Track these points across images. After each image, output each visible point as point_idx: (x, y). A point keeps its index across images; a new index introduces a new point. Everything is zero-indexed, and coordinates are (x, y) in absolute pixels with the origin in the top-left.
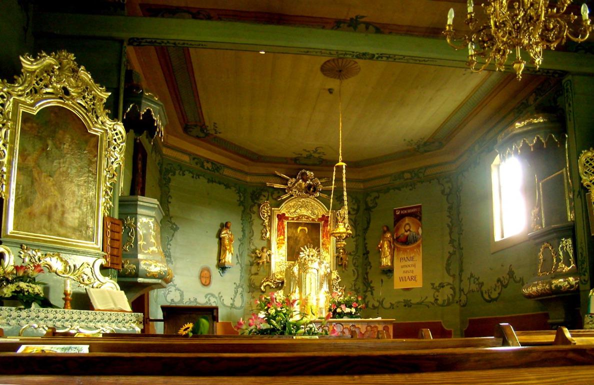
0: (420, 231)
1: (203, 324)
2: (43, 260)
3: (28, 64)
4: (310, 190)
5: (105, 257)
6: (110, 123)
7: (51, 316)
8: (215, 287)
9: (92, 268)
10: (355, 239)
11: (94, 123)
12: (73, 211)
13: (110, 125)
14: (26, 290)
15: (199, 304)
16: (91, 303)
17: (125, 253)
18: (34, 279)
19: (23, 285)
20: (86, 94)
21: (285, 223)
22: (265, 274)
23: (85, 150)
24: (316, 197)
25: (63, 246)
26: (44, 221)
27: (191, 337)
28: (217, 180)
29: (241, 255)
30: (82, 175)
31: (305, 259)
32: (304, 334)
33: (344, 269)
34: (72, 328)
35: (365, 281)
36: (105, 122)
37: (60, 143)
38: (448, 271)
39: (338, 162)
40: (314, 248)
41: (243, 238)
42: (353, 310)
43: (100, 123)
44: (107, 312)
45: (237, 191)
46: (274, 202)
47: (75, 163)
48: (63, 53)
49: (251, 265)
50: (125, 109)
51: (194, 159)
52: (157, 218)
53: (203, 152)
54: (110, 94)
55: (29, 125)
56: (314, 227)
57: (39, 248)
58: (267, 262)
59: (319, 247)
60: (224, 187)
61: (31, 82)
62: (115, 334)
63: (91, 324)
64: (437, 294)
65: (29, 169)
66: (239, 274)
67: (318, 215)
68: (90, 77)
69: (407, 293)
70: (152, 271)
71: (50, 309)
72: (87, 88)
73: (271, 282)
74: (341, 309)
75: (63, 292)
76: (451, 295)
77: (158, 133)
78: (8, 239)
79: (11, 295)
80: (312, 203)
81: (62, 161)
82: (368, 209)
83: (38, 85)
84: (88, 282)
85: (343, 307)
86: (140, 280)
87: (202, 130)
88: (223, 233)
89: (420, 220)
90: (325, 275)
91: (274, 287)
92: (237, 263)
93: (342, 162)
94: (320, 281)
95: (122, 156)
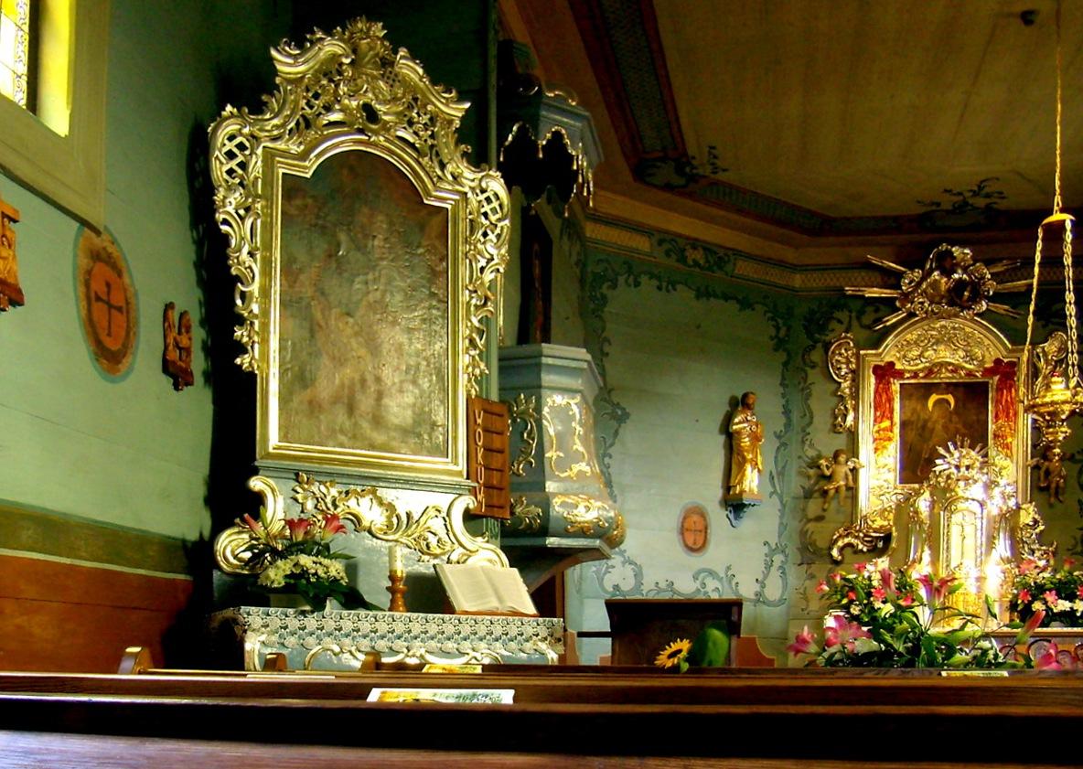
1: (715, 644)
2: (341, 505)
3: (287, 64)
4: (960, 297)
5: (473, 492)
6: (472, 176)
7: (365, 627)
8: (716, 555)
9: (447, 519)
11: (435, 179)
12: (401, 391)
13: (473, 180)
14: (313, 571)
15: (679, 594)
16: (448, 598)
17: (515, 479)
18: (327, 547)
19: (305, 560)
20: (414, 114)
21: (896, 386)
22: (841, 518)
23: (418, 247)
24: (978, 315)
25: (382, 472)
26: (341, 417)
27: (686, 673)
29: (781, 474)
30: (416, 305)
31: (949, 477)
32: (966, 665)
33: (1052, 500)
34: (410, 654)
36: (461, 175)
37: (366, 236)
39: (1050, 213)
40: (972, 447)
41: (786, 433)
43: (450, 178)
44: (483, 617)
45: (769, 315)
46: (864, 334)
47: (398, 278)
48: (360, 25)
49: (806, 497)
50: (502, 138)
51: (660, 242)
52: (586, 393)
53: (680, 224)
54: (467, 105)
55: (298, 202)
56: (972, 393)
57: (333, 477)
58: (849, 488)
59: (985, 445)
60: (738, 306)
61: (296, 102)
62: (504, 665)
63: (450, 645)
65: (304, 303)
66: (777, 521)
67: (982, 362)
68: (421, 71)
70: (579, 519)
71: (362, 612)
72: (415, 99)
73: (857, 537)
74: (1046, 603)
75: (388, 574)
77: (581, 188)
78: (269, 463)
79: (283, 584)
80: (968, 329)
81: (370, 277)
83: (311, 107)
84: (438, 551)
85: (1050, 597)
86: (552, 541)
87: (680, 170)
88: (736, 420)
91: (865, 549)
92: (771, 494)
93: (1062, 211)
95: (503, 251)
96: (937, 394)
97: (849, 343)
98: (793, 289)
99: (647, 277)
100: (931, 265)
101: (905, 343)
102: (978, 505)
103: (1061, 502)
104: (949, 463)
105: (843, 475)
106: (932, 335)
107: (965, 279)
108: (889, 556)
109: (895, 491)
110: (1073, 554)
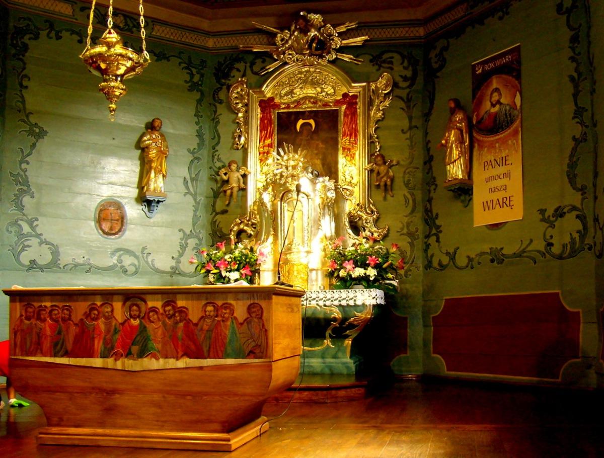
10: (408, 135)
21: (274, 117)
35: (427, 215)
42: (372, 273)
45: (184, 65)
64: (550, 231)
66: (191, 214)
69: (494, 233)
76: (578, 232)
85: (349, 266)
89: (518, 77)
96: (303, 119)
98: (207, 49)
99: (68, 34)
101: (281, 83)
105: (235, 179)
110: (401, 235)
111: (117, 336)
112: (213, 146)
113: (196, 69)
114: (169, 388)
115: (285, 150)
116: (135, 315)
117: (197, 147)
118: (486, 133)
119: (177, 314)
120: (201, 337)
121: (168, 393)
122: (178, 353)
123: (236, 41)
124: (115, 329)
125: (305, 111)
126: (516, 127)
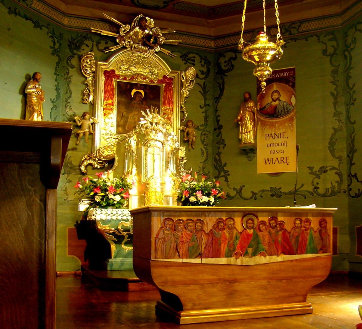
0: (293, 100)
4: (148, 42)
10: (203, 110)
22: (86, 150)
24: (156, 53)
28: (22, 13)
31: (147, 128)
33: (190, 147)
35: (217, 163)
38: (332, 151)
42: (212, 199)
46: (100, 54)
64: (317, 180)
69: (274, 178)
73: (95, 160)
74: (196, 198)
76: (337, 182)
82: (221, 73)
85: (199, 194)
88: (30, 87)
89: (293, 86)
90: (172, 151)
94: (166, 160)
97: (92, 57)
98: (64, 25)
100: (135, 24)
101: (120, 61)
102: (161, 144)
103: (193, 148)
104: (147, 120)
105: (87, 126)
106: (133, 60)
107: (151, 34)
108: (113, 170)
109: (115, 137)
111: (238, 242)
112: (66, 99)
113: (57, 39)
114: (271, 276)
115: (151, 110)
116: (250, 226)
117: (55, 98)
118: (268, 117)
119: (278, 226)
120: (293, 242)
121: (271, 279)
122: (278, 251)
123: (85, 24)
124: (236, 237)
125: (138, 84)
126: (292, 116)
